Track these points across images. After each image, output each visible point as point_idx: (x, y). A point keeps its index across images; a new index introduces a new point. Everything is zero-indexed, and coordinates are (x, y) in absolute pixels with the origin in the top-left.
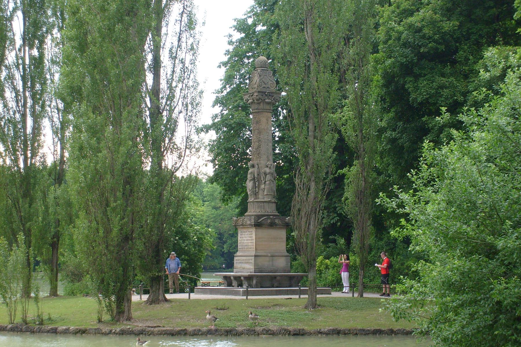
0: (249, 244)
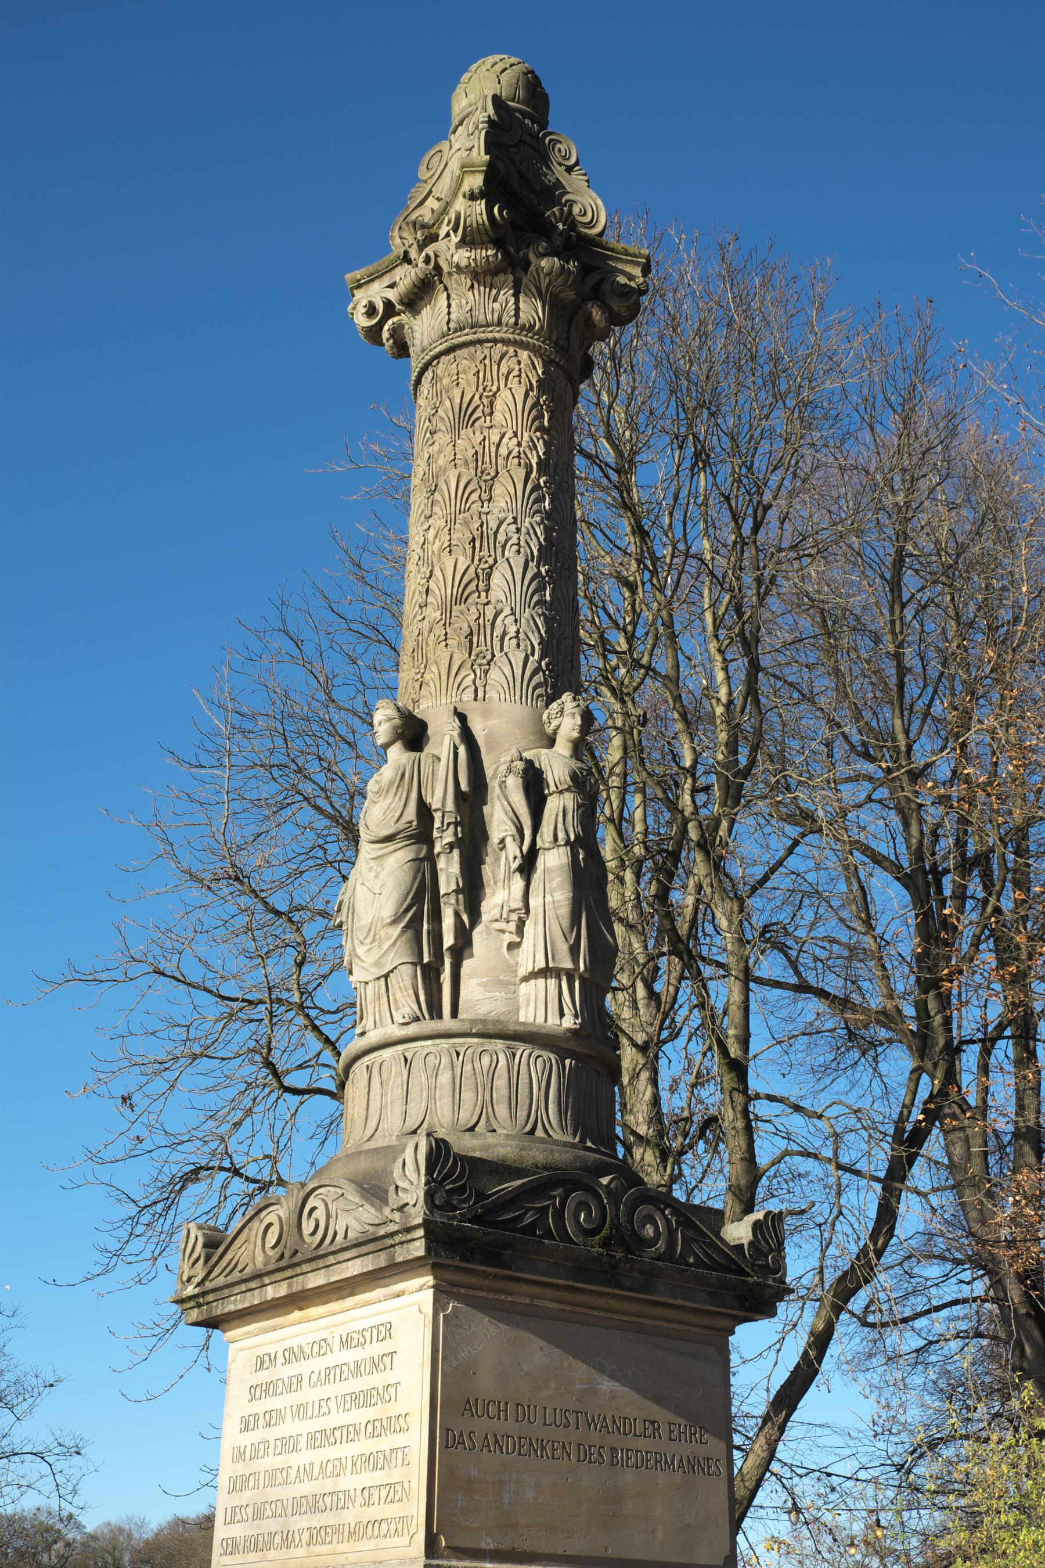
0: (350, 1482)
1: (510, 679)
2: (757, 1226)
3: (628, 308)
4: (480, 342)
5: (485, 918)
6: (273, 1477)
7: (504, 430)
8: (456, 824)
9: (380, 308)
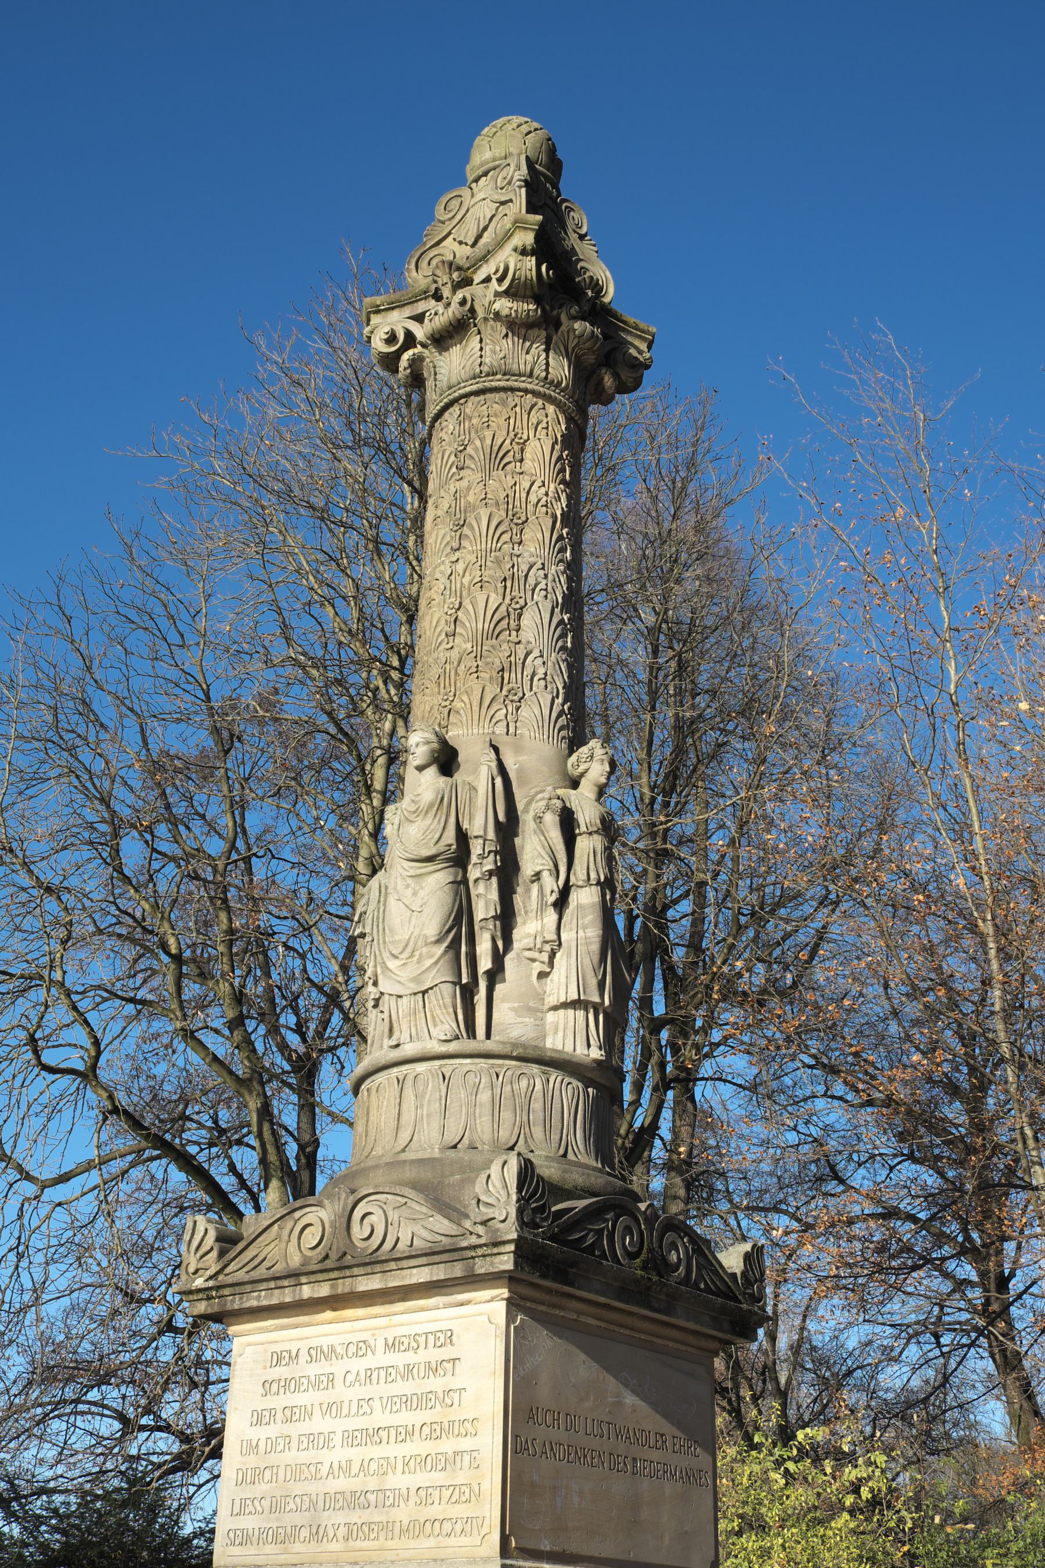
0: (398, 1481)
1: (540, 719)
2: (747, 1257)
3: (635, 379)
4: (512, 390)
5: (516, 945)
6: (297, 1472)
7: (534, 478)
9: (401, 337)
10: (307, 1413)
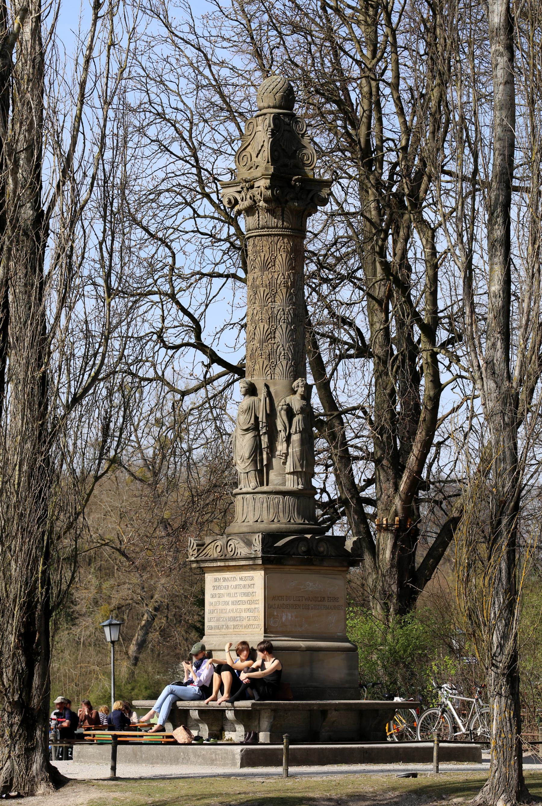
0: (244, 615)
6: (222, 611)
8: (266, 426)
10: (223, 595)
